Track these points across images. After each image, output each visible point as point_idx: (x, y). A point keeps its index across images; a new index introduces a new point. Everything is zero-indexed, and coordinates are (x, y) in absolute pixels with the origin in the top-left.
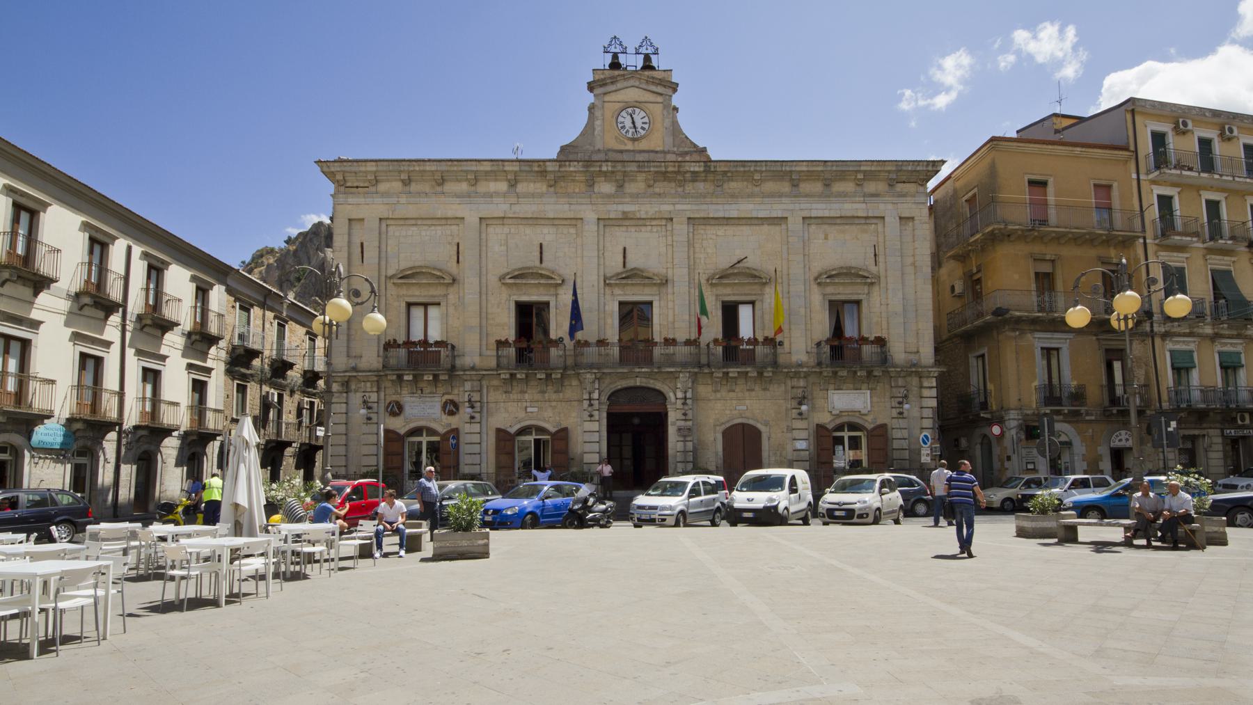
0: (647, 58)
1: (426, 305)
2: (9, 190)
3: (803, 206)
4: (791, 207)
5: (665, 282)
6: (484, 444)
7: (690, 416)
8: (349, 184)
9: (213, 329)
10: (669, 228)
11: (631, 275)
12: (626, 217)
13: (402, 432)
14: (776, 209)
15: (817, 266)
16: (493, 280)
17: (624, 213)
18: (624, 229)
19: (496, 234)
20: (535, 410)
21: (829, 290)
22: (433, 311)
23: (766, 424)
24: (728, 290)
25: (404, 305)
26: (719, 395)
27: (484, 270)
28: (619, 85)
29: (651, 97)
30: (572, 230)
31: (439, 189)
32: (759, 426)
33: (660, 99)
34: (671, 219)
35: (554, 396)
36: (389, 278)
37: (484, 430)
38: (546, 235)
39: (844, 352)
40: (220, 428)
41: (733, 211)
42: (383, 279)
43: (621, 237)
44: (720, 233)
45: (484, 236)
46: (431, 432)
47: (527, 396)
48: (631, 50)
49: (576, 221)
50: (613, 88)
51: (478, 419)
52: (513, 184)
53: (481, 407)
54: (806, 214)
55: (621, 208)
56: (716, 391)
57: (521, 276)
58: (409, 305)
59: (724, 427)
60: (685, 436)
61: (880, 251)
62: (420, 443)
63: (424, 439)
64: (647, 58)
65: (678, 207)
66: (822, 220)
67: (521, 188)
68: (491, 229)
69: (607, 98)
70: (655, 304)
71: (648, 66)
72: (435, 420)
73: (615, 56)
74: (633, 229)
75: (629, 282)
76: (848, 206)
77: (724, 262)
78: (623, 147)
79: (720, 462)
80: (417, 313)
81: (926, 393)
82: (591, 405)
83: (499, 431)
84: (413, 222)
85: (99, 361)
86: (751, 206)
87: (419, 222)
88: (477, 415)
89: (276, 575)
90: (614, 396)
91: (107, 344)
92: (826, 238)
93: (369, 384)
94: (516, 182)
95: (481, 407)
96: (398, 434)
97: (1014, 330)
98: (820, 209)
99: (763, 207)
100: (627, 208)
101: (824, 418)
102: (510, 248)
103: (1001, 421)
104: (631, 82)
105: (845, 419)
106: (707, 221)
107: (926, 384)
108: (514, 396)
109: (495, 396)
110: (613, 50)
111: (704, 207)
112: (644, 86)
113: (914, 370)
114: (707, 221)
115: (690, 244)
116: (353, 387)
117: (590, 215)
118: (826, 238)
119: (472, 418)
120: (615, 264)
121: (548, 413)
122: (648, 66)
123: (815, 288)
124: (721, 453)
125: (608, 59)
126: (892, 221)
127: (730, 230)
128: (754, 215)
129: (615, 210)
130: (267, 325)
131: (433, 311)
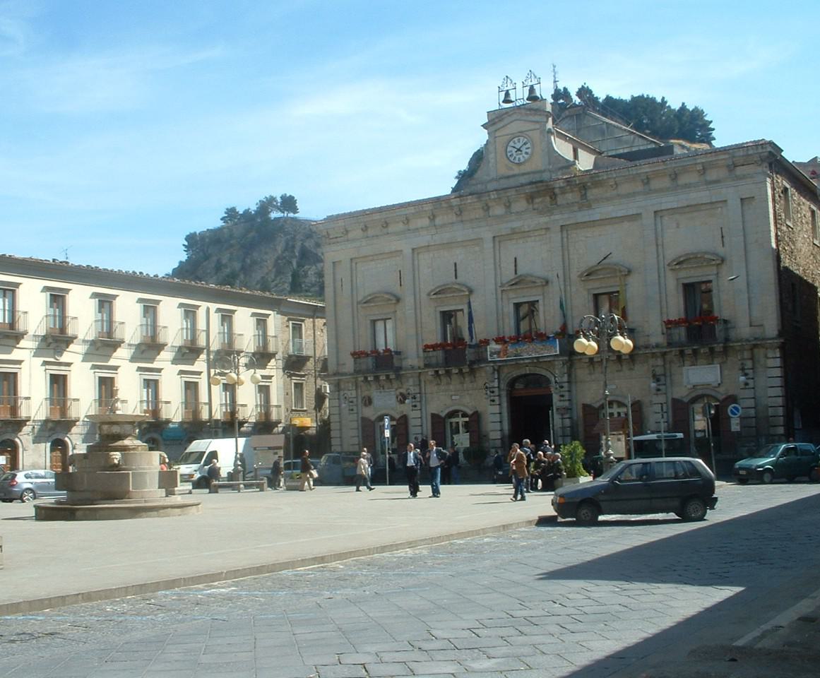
2: (140, 301)
6: (424, 426)
8: (331, 237)
9: (271, 349)
11: (519, 281)
12: (514, 232)
13: (373, 418)
15: (672, 253)
16: (424, 296)
18: (514, 242)
19: (425, 259)
20: (458, 397)
21: (682, 274)
22: (390, 324)
24: (596, 284)
26: (593, 377)
27: (417, 290)
28: (505, 122)
29: (532, 126)
30: (477, 249)
31: (385, 231)
33: (537, 126)
35: (470, 386)
36: (358, 303)
37: (424, 415)
38: (459, 255)
39: (699, 327)
42: (355, 304)
43: (512, 250)
45: (416, 263)
46: (464, 415)
47: (451, 387)
49: (478, 241)
50: (501, 124)
51: (751, 385)
52: (433, 218)
53: (421, 397)
54: (655, 209)
56: (590, 374)
57: (440, 292)
60: (562, 415)
62: (458, 423)
63: (461, 420)
66: (673, 211)
67: (438, 221)
68: (421, 256)
69: (498, 134)
72: (393, 409)
73: (507, 94)
74: (521, 241)
75: (518, 287)
77: (593, 260)
78: (511, 173)
81: (771, 363)
83: (433, 416)
84: (371, 258)
85: (196, 384)
86: (611, 208)
87: (375, 258)
88: (750, 382)
90: (512, 383)
91: (199, 373)
92: (678, 227)
93: (350, 385)
94: (434, 217)
95: (421, 397)
96: (370, 420)
100: (516, 224)
101: (681, 392)
102: (433, 271)
104: (515, 117)
105: (700, 392)
106: (578, 225)
107: (770, 355)
108: (443, 388)
109: (430, 389)
110: (506, 89)
112: (525, 118)
113: (756, 345)
114: (578, 225)
116: (342, 387)
117: (487, 235)
118: (678, 227)
119: (746, 384)
120: (509, 274)
121: (467, 400)
123: (669, 274)
125: (502, 95)
128: (614, 215)
129: (504, 228)
130: (318, 333)
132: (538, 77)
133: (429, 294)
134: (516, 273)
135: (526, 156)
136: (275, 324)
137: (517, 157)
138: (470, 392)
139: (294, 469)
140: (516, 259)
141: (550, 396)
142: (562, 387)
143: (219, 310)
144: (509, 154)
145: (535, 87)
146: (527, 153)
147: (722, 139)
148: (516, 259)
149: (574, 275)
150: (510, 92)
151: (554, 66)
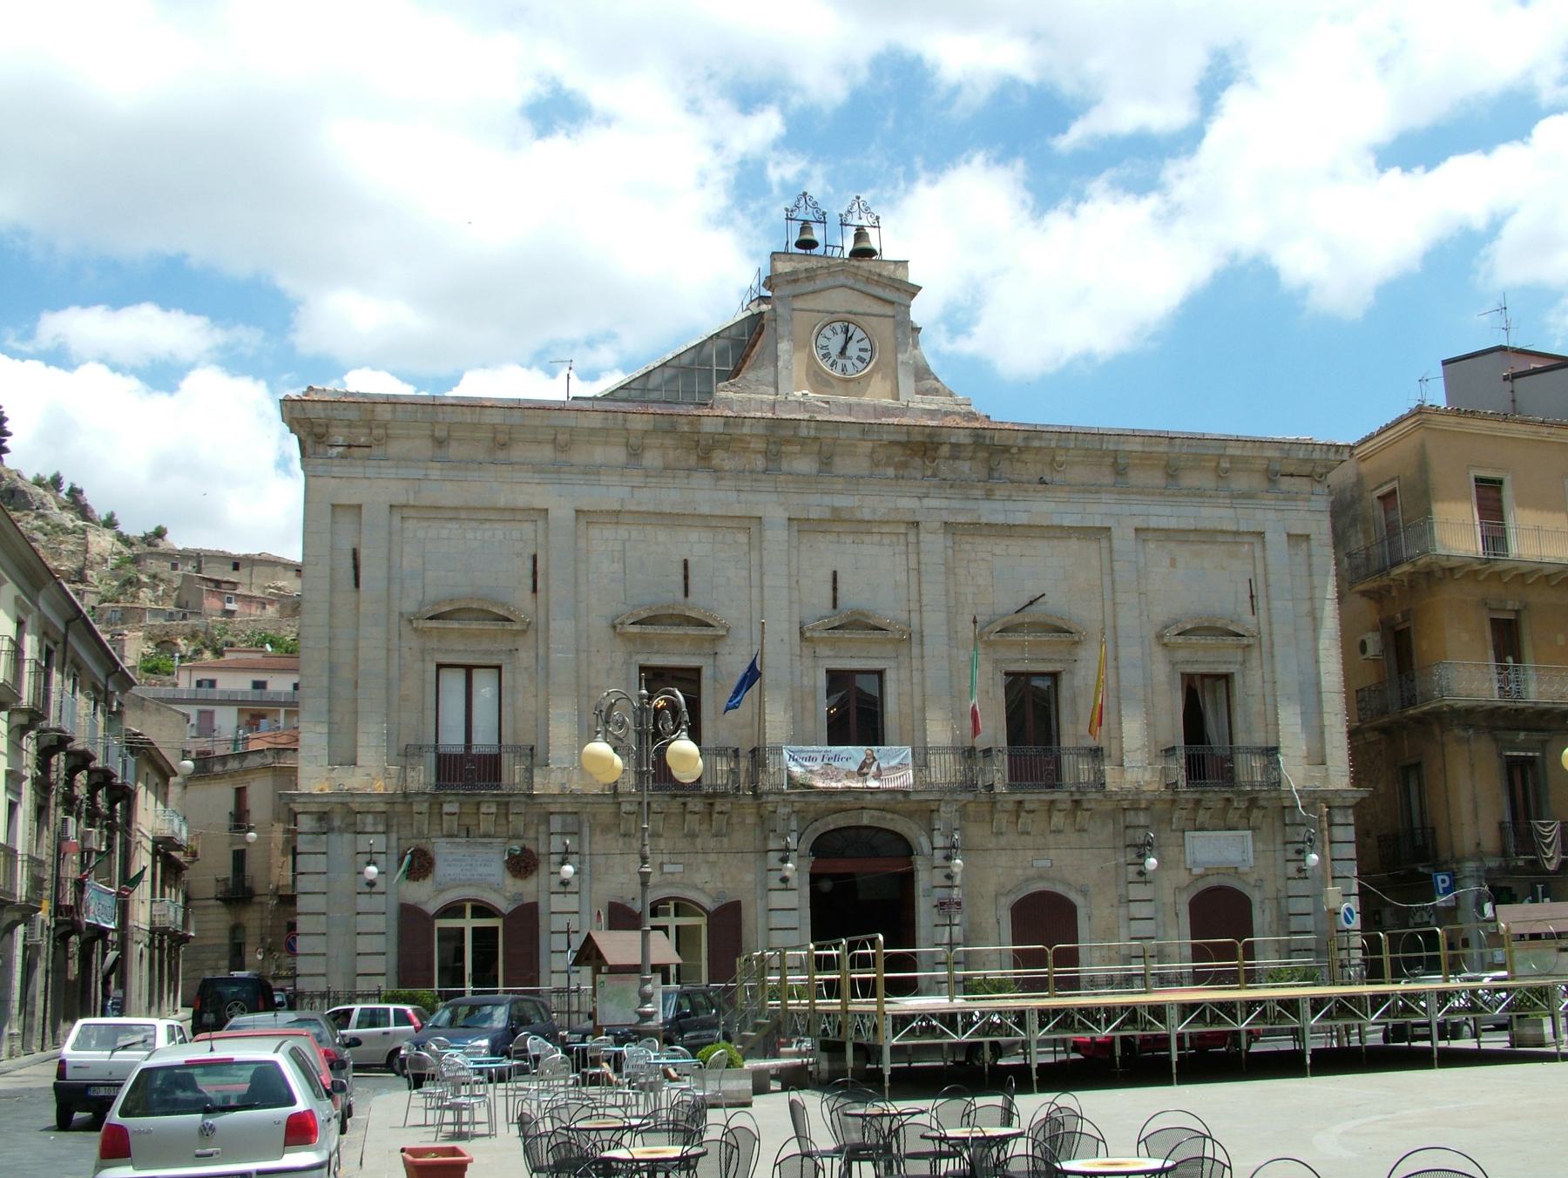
0: (860, 234)
3: (1136, 509)
14: (1094, 513)
20: (680, 868)
23: (1084, 892)
38: (695, 544)
48: (833, 220)
59: (1015, 898)
64: (860, 234)
127: (1016, 546)
140: (835, 573)
148: (835, 573)
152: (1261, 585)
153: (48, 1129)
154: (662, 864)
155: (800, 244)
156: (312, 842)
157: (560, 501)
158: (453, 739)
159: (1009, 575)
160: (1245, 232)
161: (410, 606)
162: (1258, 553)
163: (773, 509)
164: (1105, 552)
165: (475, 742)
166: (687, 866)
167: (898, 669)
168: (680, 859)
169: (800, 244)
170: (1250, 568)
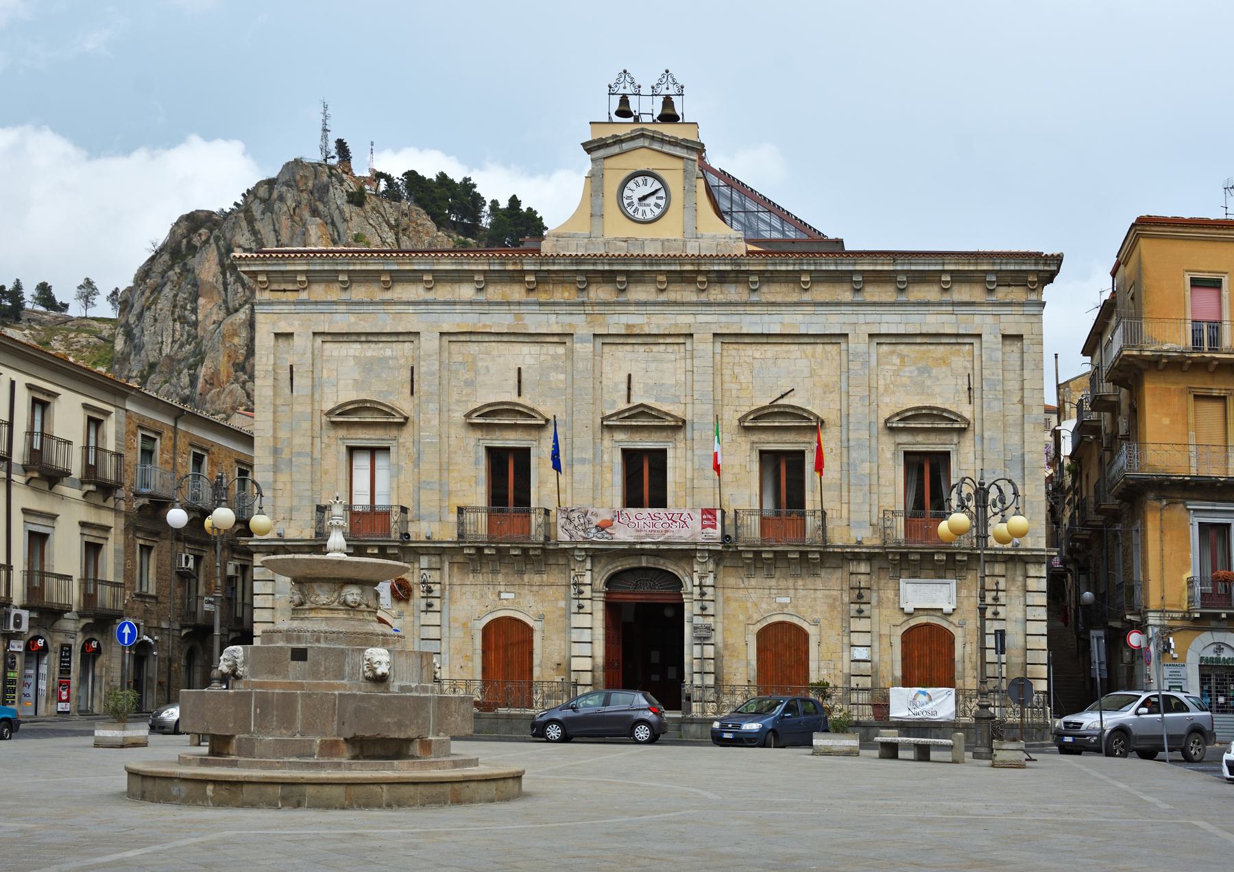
0: (668, 102)
1: (373, 451)
3: (870, 319)
4: (853, 319)
5: (679, 426)
7: (710, 611)
10: (689, 347)
11: (639, 416)
14: (832, 322)
17: (628, 326)
20: (511, 596)
23: (816, 623)
25: (344, 450)
32: (805, 626)
34: (691, 335)
38: (526, 355)
40: (120, 607)
41: (773, 323)
44: (757, 355)
48: (646, 90)
53: (442, 591)
55: (624, 319)
58: (352, 450)
59: (759, 626)
61: (976, 385)
64: (668, 102)
65: (701, 318)
70: (670, 454)
71: (669, 117)
73: (624, 100)
76: (931, 319)
79: (753, 673)
80: (362, 462)
82: (703, 594)
89: (717, 557)
97: (1159, 499)
98: (892, 322)
99: (815, 319)
103: (1142, 627)
110: (622, 91)
111: (736, 318)
115: (717, 370)
122: (669, 117)
124: (754, 663)
125: (615, 103)
126: (991, 339)
127: (770, 351)
131: (381, 462)
132: (637, 83)
133: (468, 416)
134: (629, 402)
135: (655, 209)
136: (117, 432)
137: (641, 209)
138: (535, 588)
139: (1166, 712)
140: (630, 376)
141: (680, 607)
142: (581, 592)
143: (30, 387)
144: (626, 202)
145: (674, 99)
146: (657, 206)
147: (847, 248)
148: (630, 376)
149: (731, 418)
150: (630, 98)
151: (326, 107)
152: (977, 379)
153: (119, 796)
154: (500, 592)
155: (618, 113)
156: (263, 573)
157: (429, 324)
158: (361, 500)
159: (905, 384)
160: (74, 292)
161: (329, 406)
162: (976, 352)
163: (580, 324)
164: (844, 354)
165: (377, 503)
166: (518, 595)
167: (675, 448)
168: (512, 588)
169: (618, 113)
170: (969, 365)
